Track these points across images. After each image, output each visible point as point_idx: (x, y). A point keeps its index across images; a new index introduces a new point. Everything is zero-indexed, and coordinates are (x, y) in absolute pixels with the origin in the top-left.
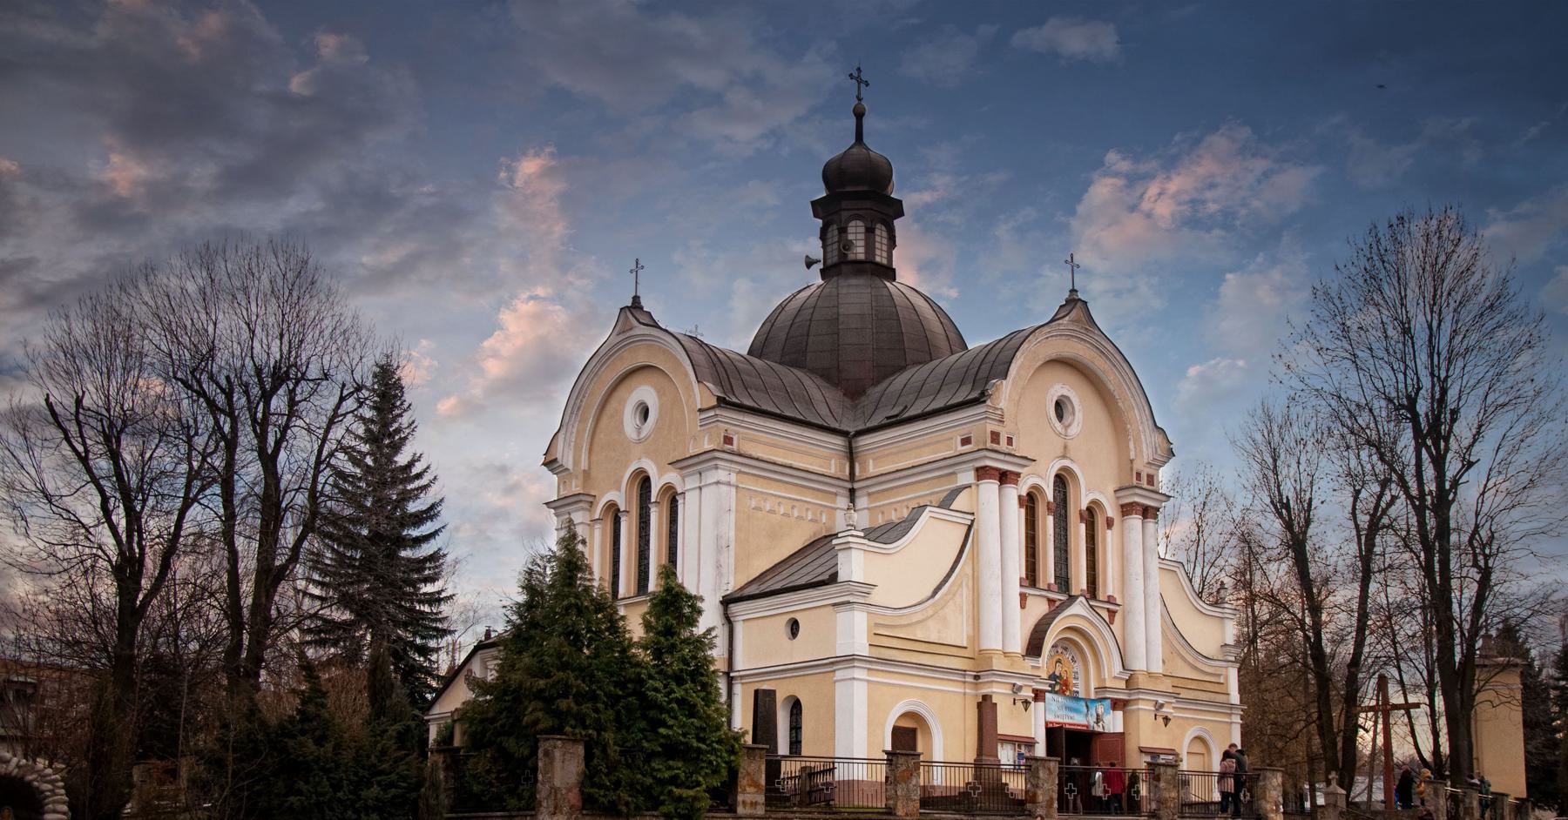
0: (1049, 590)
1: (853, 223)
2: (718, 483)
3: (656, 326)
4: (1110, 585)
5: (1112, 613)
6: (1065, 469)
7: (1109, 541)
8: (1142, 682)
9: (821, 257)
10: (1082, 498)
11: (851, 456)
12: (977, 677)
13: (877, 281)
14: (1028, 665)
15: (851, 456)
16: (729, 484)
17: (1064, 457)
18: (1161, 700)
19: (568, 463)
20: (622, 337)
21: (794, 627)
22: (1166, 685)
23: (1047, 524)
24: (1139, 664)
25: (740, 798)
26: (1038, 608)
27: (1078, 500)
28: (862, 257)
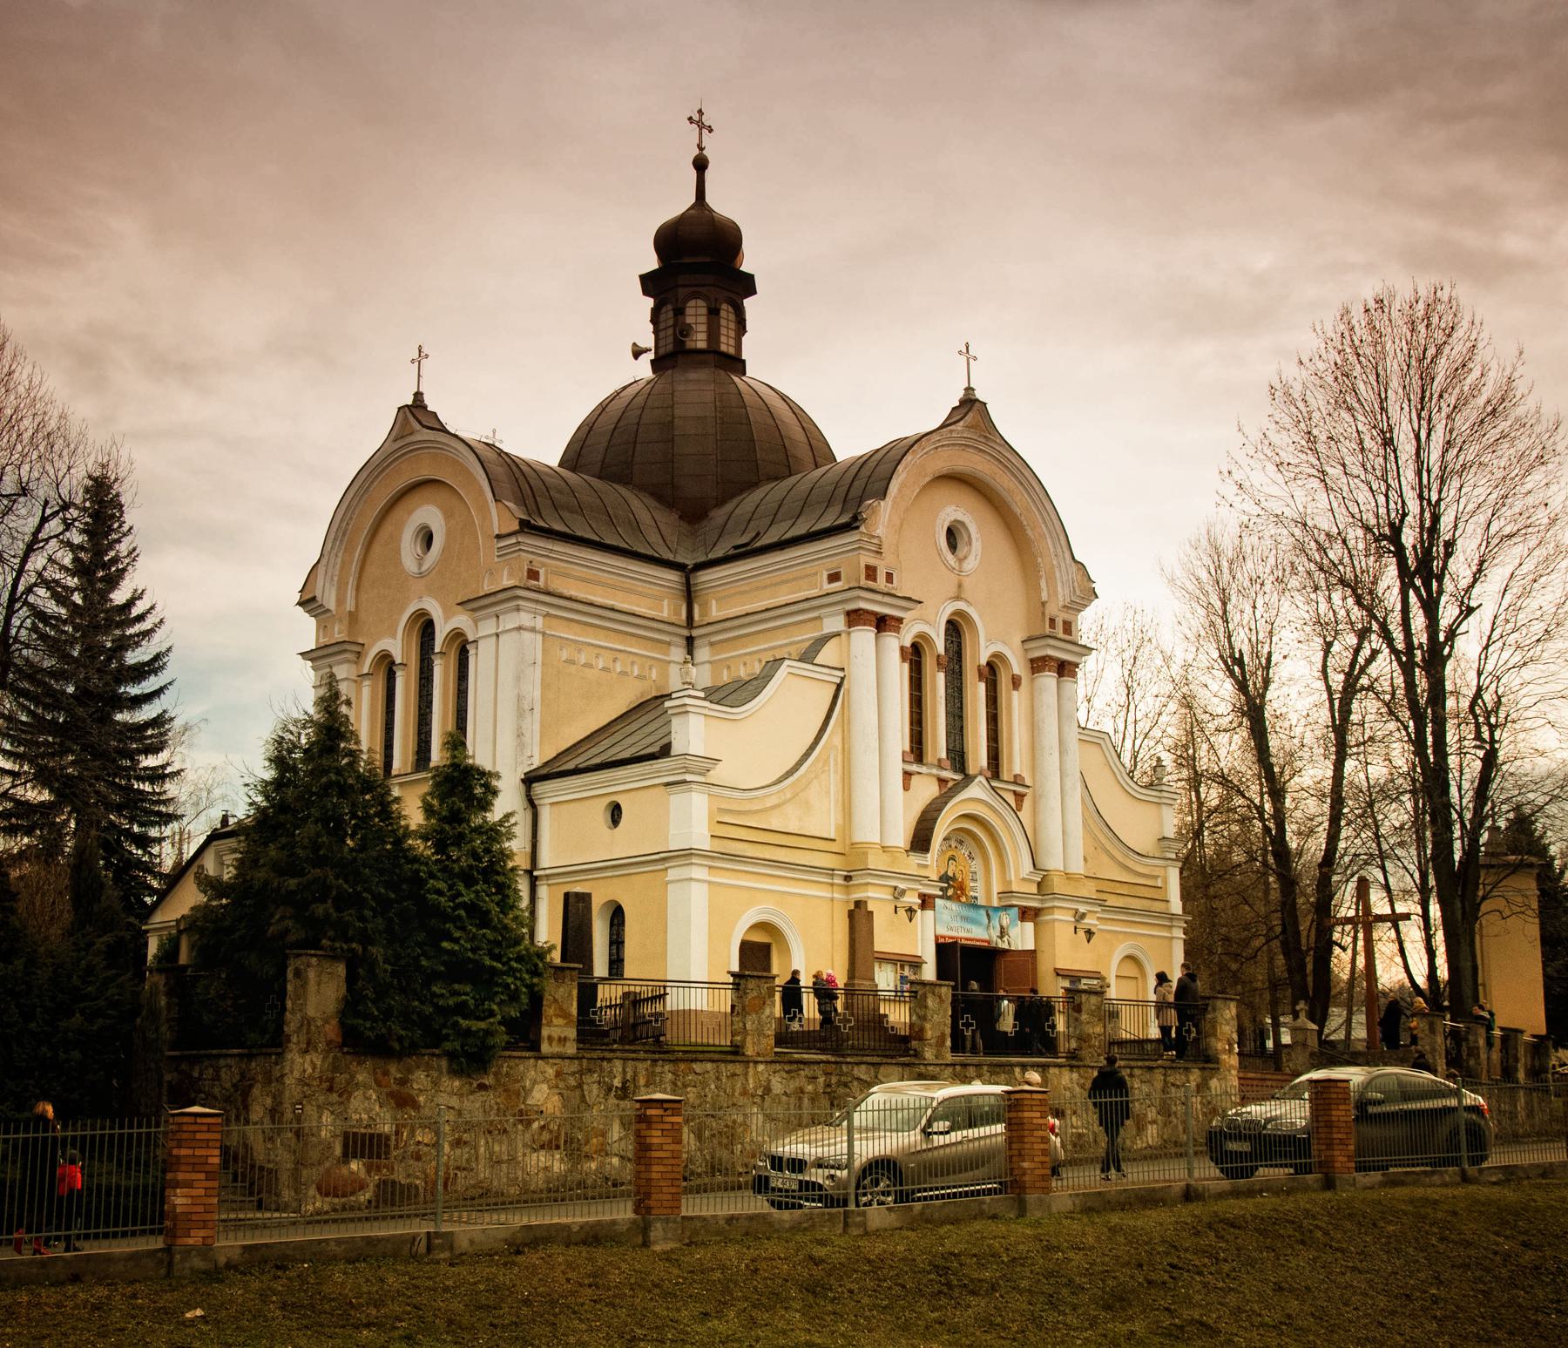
1: (692, 303)
2: (519, 628)
4: (1016, 761)
5: (1019, 797)
7: (1015, 704)
8: (1058, 885)
10: (980, 651)
12: (848, 878)
16: (533, 630)
17: (958, 598)
19: (330, 602)
20: (400, 443)
21: (615, 813)
24: (1054, 862)
25: (545, 1032)
26: (926, 790)
28: (702, 345)
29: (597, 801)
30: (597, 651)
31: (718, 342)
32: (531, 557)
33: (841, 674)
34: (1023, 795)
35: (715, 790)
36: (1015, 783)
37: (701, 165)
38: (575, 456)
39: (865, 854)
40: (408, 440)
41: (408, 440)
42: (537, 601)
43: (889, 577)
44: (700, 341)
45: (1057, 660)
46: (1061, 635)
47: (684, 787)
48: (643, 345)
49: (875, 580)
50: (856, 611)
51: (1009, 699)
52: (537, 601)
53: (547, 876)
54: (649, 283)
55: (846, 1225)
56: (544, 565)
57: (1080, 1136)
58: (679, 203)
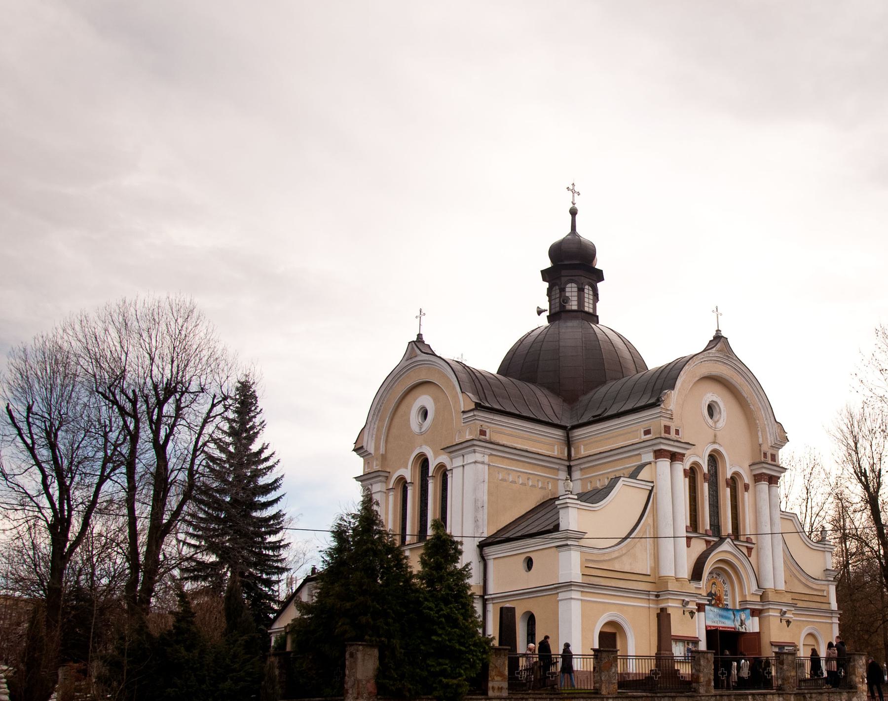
1: (569, 285)
5: (750, 550)
6: (715, 451)
8: (771, 597)
10: (728, 471)
11: (569, 443)
15: (569, 443)
16: (483, 463)
17: (714, 442)
18: (784, 609)
19: (371, 449)
21: (529, 563)
24: (769, 584)
25: (490, 685)
26: (699, 546)
27: (725, 472)
28: (575, 308)
31: (584, 306)
37: (573, 212)
38: (506, 367)
40: (414, 360)
41: (414, 360)
43: (677, 432)
46: (770, 462)
48: (543, 308)
49: (669, 433)
53: (493, 599)
54: (546, 275)
56: (489, 427)
58: (561, 232)
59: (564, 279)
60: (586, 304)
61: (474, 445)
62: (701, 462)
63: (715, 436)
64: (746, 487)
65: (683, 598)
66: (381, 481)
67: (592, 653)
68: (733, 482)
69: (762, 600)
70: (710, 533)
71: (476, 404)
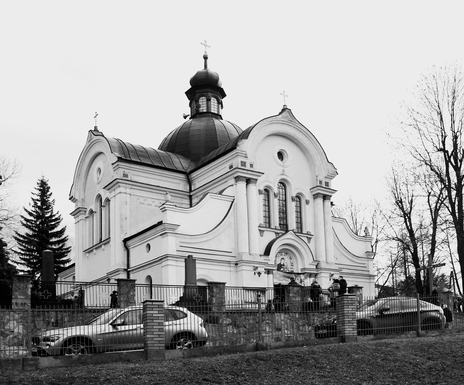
0: (276, 229)
1: (201, 98)
2: (120, 193)
3: (103, 136)
4: (308, 227)
5: (309, 239)
6: (283, 179)
7: (307, 210)
8: (323, 265)
9: (190, 114)
10: (292, 192)
11: (190, 182)
12: (236, 264)
13: (210, 118)
14: (263, 259)
15: (190, 182)
16: (126, 193)
17: (283, 174)
19: (77, 197)
20: (90, 143)
21: (149, 246)
22: (336, 267)
23: (275, 204)
24: (322, 259)
25: (14, 301)
26: (269, 236)
28: (205, 111)
29: (143, 244)
30: (153, 200)
31: (211, 110)
32: (124, 170)
33: (233, 198)
34: (311, 238)
35: (177, 235)
36: (307, 234)
37: (206, 58)
38: (161, 148)
39: (242, 256)
40: (91, 141)
41: (91, 141)
42: (126, 184)
43: (251, 166)
44: (203, 109)
45: (323, 194)
46: (324, 186)
47: (166, 235)
48: (187, 114)
49: (245, 166)
50: (238, 177)
51: (305, 208)
52: (126, 184)
53: (132, 270)
54: (188, 93)
55: (23, 365)
57: (289, 337)
59: (197, 95)
60: (212, 108)
61: (118, 182)
62: (272, 185)
63: (283, 171)
64: (307, 202)
65: (254, 265)
66: (82, 214)
67: (116, 282)
68: (298, 197)
69: (316, 268)
70: (279, 228)
71: (118, 158)
